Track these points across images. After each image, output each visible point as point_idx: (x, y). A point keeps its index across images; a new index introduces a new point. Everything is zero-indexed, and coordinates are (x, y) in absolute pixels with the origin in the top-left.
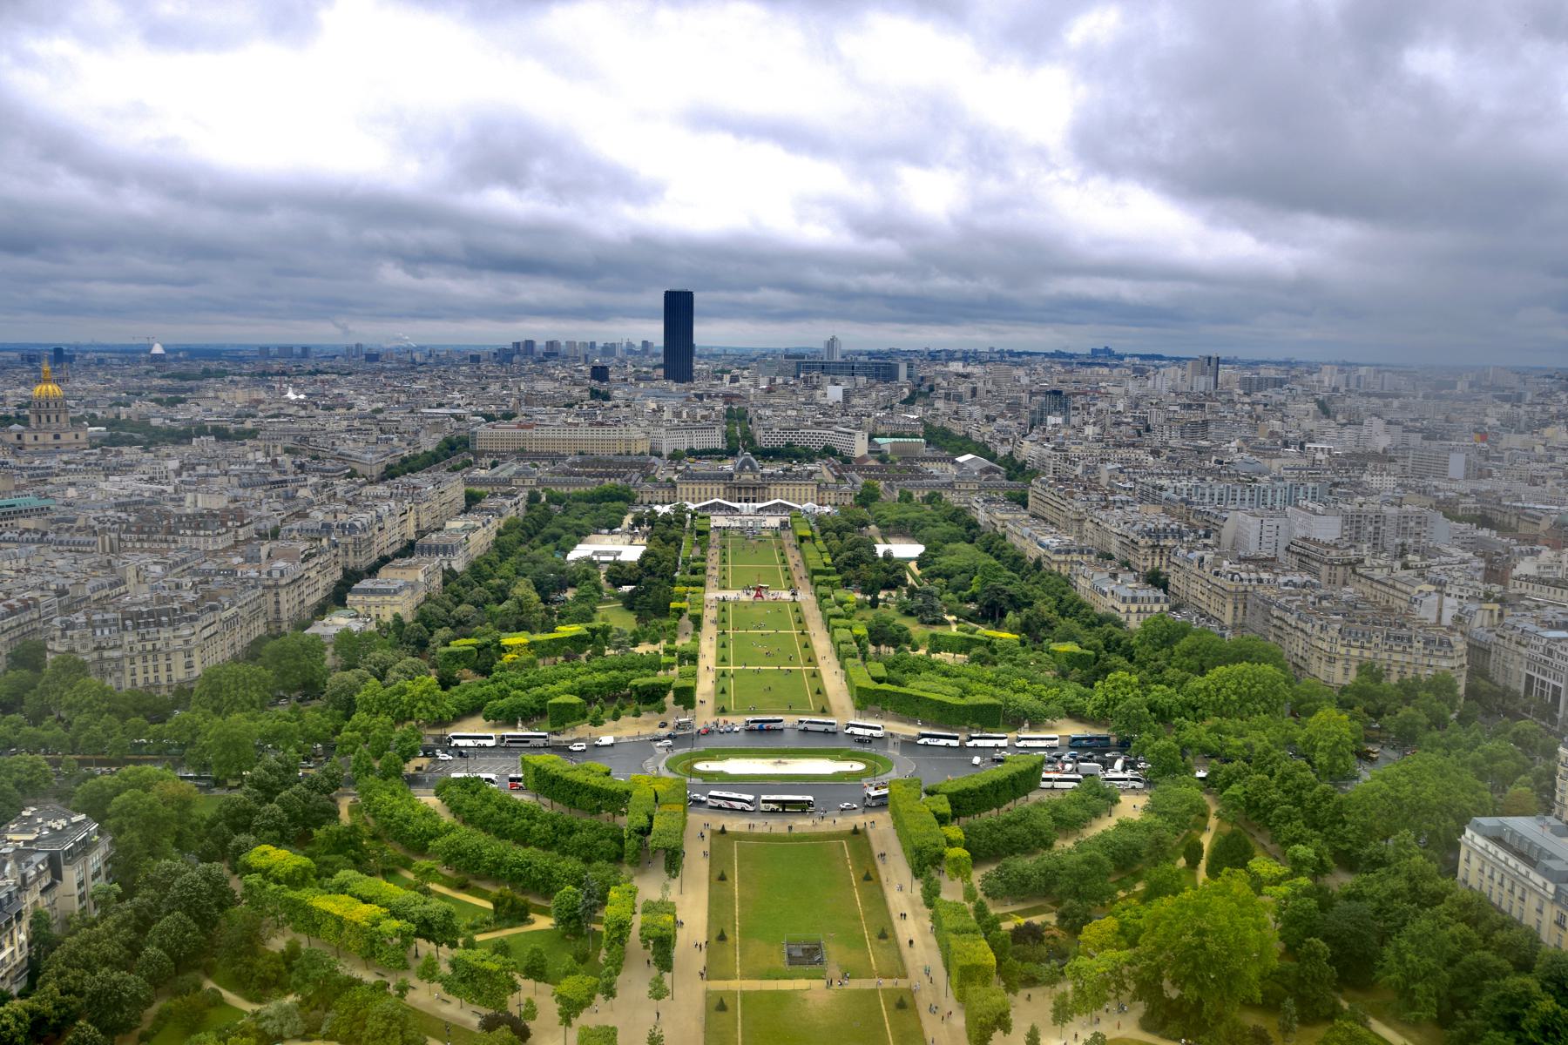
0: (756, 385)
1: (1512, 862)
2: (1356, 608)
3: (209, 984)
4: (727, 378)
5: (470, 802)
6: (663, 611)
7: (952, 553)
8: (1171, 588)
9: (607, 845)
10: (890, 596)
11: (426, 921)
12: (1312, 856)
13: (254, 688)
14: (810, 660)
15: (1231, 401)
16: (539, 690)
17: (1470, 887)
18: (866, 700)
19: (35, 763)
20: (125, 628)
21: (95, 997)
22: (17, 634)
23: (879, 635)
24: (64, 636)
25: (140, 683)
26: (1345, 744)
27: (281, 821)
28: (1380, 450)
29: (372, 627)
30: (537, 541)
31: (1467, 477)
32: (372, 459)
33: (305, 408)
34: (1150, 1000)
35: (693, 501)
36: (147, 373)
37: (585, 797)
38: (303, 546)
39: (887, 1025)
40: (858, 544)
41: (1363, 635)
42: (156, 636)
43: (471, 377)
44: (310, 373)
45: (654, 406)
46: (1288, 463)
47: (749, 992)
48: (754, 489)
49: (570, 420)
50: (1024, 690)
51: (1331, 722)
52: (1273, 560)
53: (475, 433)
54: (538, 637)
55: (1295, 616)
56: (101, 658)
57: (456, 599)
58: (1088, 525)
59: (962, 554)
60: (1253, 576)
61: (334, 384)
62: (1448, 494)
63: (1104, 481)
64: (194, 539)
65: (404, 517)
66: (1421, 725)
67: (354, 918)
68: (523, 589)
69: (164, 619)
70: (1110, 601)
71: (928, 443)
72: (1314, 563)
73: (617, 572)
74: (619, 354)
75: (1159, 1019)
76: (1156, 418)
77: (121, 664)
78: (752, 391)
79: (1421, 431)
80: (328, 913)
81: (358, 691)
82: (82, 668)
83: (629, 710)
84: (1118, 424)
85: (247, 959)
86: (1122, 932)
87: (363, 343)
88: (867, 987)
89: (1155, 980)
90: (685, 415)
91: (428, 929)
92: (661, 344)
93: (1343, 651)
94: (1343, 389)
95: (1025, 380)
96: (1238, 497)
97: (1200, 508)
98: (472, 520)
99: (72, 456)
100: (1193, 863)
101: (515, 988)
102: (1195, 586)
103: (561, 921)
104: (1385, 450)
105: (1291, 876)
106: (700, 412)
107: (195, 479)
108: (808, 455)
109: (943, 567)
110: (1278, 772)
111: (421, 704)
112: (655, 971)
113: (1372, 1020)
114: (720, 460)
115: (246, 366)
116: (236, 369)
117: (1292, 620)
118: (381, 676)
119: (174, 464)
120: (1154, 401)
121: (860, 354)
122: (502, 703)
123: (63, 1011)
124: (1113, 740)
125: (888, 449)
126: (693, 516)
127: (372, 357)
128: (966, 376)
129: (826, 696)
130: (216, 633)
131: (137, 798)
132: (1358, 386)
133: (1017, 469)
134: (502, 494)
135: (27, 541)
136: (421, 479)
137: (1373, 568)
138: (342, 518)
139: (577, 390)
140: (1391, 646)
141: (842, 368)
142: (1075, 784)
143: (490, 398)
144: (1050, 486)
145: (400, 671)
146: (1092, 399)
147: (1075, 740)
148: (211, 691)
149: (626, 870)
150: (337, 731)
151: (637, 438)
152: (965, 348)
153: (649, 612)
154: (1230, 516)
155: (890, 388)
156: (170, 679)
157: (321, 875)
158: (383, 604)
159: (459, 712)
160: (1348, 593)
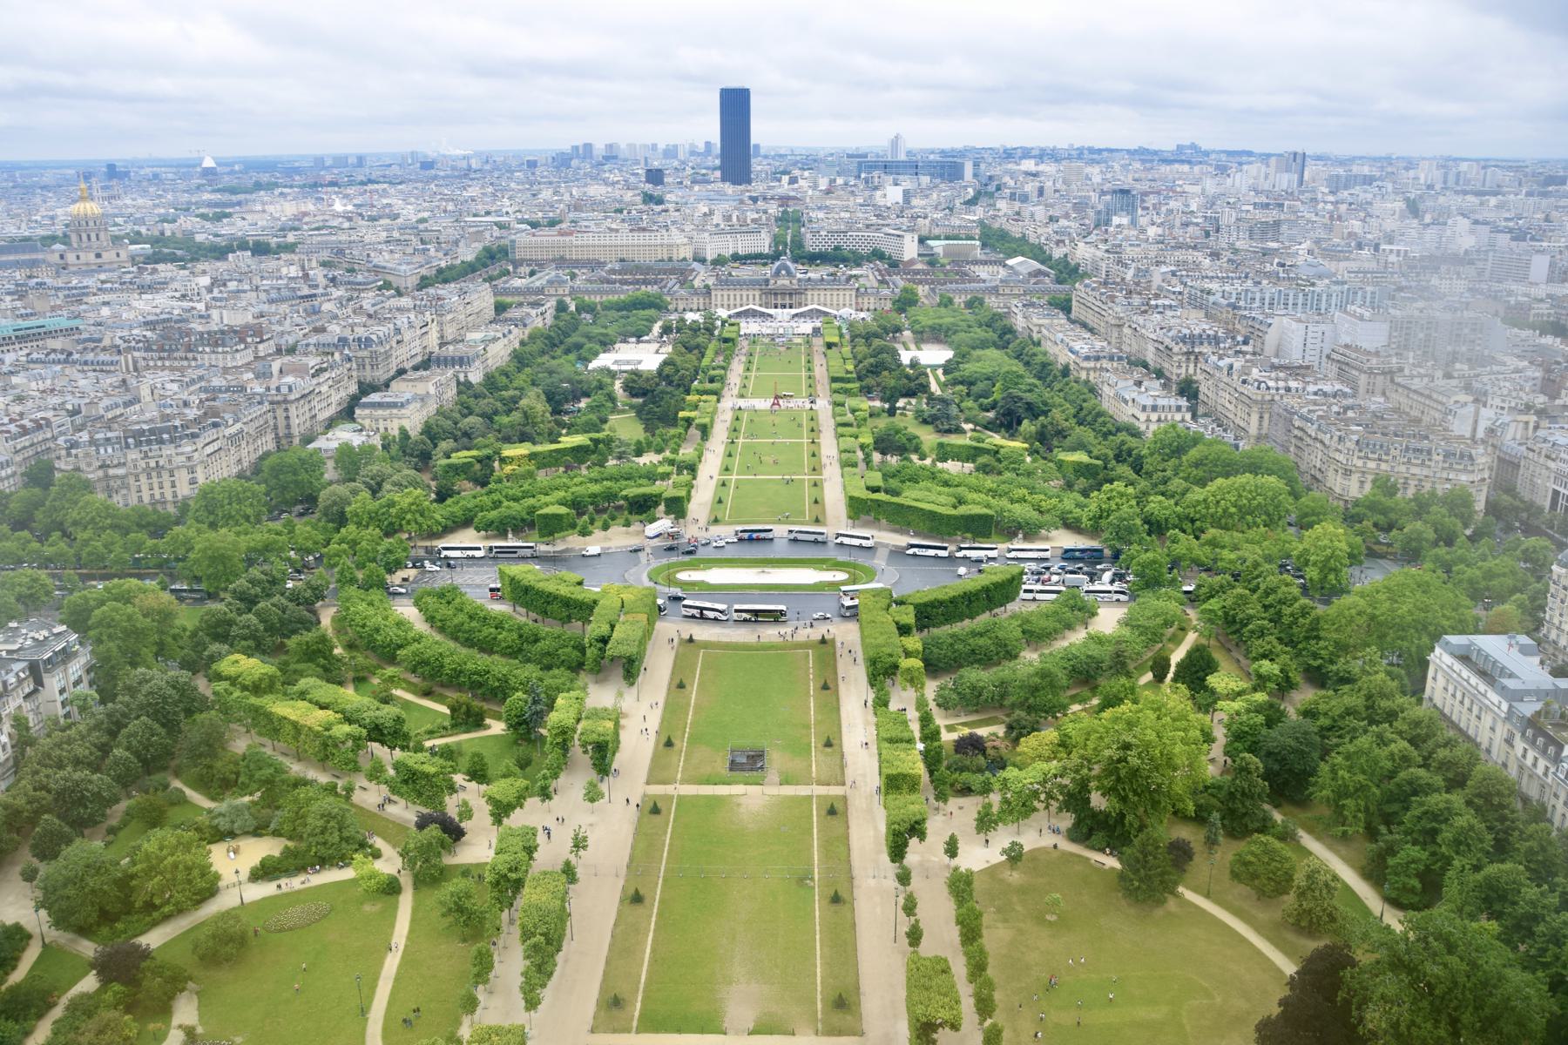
0: (815, 186)
1: (1474, 680)
2: (1382, 418)
3: (177, 784)
4: (786, 179)
5: (445, 611)
6: (672, 421)
7: (979, 359)
8: (1201, 396)
10: (910, 404)
11: (377, 725)
12: (1277, 672)
13: (247, 503)
14: (814, 470)
15: (1314, 200)
16: (531, 501)
17: (1435, 706)
19: (35, 576)
20: (128, 446)
21: (60, 795)
22: (31, 453)
23: (885, 444)
24: (69, 455)
25: (146, 499)
26: (1338, 559)
27: (257, 630)
28: (1462, 252)
29: (377, 441)
30: (559, 352)
31: (1550, 280)
32: (407, 271)
33: (350, 219)
34: (1075, 811)
35: (729, 308)
36: (198, 188)
37: (555, 607)
38: (313, 361)
39: (815, 830)
40: (881, 350)
41: (1381, 446)
42: (159, 453)
43: (523, 183)
44: (363, 183)
45: (706, 210)
46: (1354, 266)
48: (791, 294)
49: (614, 226)
50: (1023, 500)
51: (1331, 536)
52: (1308, 367)
53: (513, 241)
54: (539, 448)
55: (1315, 427)
56: (107, 476)
57: (466, 411)
58: (1126, 330)
60: (1281, 384)
61: (385, 194)
62: (1520, 298)
63: (1157, 280)
64: (213, 356)
65: (424, 330)
66: (1427, 540)
67: (308, 723)
68: (534, 401)
69: (165, 436)
70: (1130, 410)
71: (984, 246)
72: (1354, 372)
73: (634, 381)
74: (681, 156)
75: (1085, 830)
76: (1228, 217)
77: (126, 481)
79: (1511, 231)
81: (349, 504)
82: (88, 486)
83: (621, 521)
84: (1186, 225)
85: (207, 761)
86: (1063, 744)
88: (803, 793)
89: (1080, 792)
91: (377, 733)
92: (719, 145)
93: (1360, 463)
94: (1438, 187)
95: (1097, 179)
96: (1291, 302)
97: (1246, 313)
98: (496, 330)
100: (1160, 677)
101: (452, 789)
102: (1224, 394)
103: (510, 726)
104: (1466, 252)
105: (1255, 690)
106: (751, 215)
108: (856, 260)
109: (967, 373)
110: (1263, 586)
111: (409, 516)
112: (593, 775)
113: (1301, 832)
114: (765, 264)
115: (297, 178)
116: (288, 181)
117: (1312, 430)
118: (375, 490)
119: (205, 281)
120: (1232, 200)
121: (933, 153)
122: (493, 514)
123: (35, 805)
124: (1107, 552)
125: (940, 251)
126: (724, 322)
127: (428, 165)
128: (1035, 175)
129: (824, 505)
131: (116, 610)
132: (1457, 183)
133: (1068, 272)
135: (54, 362)
136: (449, 292)
137: (1412, 377)
138: (361, 332)
139: (630, 193)
140: (1409, 459)
142: (1054, 596)
143: (538, 205)
144: (1093, 289)
145: (395, 484)
146: (1165, 198)
147: (1067, 551)
149: (583, 678)
150: (328, 543)
151: (678, 242)
152: (1043, 145)
153: (656, 422)
154: (1275, 321)
155: (954, 188)
156: (175, 495)
157: (281, 684)
158: (391, 417)
159: (449, 523)
160: (1376, 402)
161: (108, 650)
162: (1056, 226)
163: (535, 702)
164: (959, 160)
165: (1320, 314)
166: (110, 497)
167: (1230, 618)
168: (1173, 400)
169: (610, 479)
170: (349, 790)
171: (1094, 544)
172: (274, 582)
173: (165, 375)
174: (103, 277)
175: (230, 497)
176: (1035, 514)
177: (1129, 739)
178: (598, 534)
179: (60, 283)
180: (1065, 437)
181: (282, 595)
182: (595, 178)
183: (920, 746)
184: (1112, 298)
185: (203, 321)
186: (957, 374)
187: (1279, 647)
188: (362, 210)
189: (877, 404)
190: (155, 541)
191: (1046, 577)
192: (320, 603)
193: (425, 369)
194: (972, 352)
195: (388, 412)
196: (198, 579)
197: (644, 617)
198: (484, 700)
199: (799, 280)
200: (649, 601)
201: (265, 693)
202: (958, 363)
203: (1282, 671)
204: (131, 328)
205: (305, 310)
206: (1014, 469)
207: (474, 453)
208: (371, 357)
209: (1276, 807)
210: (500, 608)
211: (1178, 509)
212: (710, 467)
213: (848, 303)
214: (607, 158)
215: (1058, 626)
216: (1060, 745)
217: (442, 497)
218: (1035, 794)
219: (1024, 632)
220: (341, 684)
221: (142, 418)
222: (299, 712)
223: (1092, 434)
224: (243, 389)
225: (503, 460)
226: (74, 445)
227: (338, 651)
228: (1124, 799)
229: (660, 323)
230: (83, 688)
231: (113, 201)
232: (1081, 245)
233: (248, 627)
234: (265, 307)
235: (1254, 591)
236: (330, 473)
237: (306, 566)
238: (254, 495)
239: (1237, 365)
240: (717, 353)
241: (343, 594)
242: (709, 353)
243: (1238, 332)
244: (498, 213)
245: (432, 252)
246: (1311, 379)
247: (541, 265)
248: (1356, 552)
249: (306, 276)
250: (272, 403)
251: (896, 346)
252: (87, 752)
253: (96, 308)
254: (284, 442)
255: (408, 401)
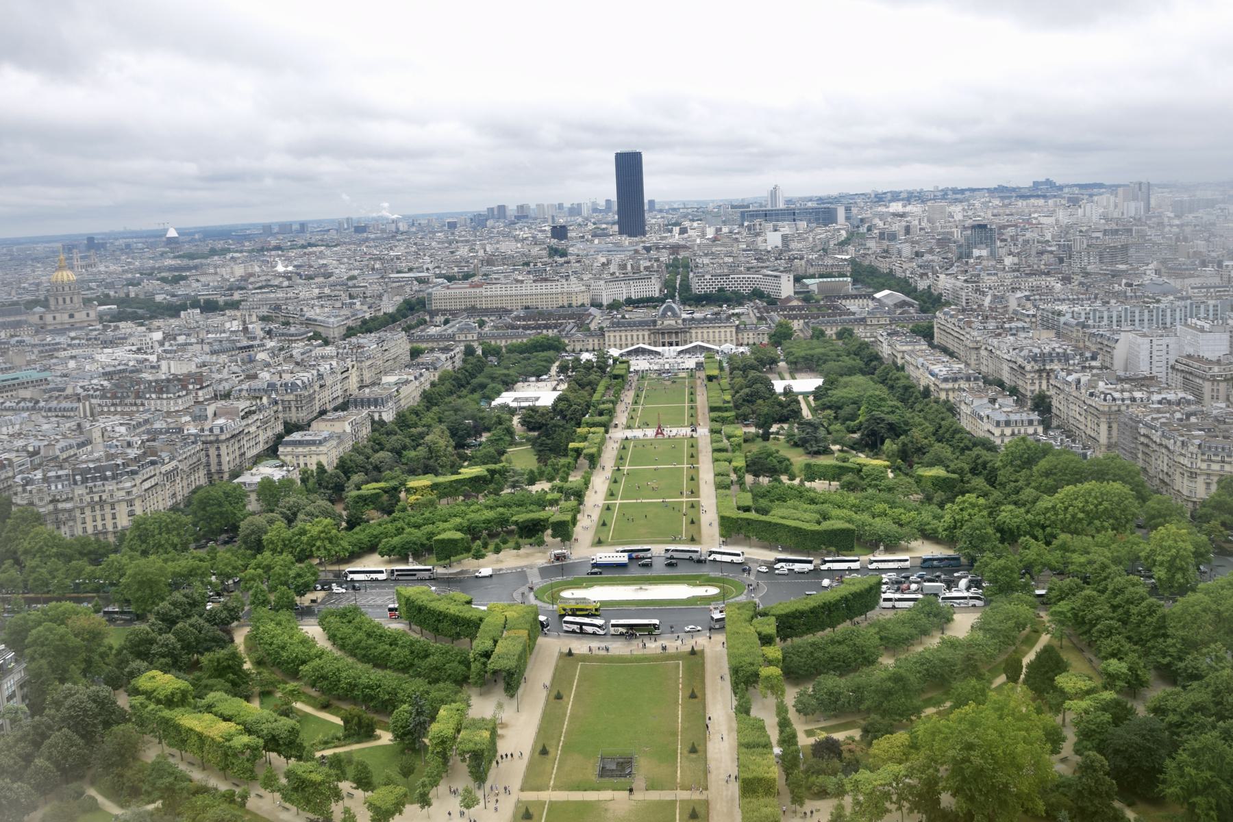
0: (703, 235)
2: (1225, 423)
3: (92, 792)
4: (676, 229)
5: (346, 629)
7: (846, 385)
8: (1054, 410)
9: (455, 667)
10: (782, 428)
11: (274, 736)
16: (429, 528)
18: (731, 529)
20: (75, 483)
24: (24, 491)
25: (90, 530)
26: (1183, 558)
27: (174, 649)
29: (296, 476)
30: (465, 392)
32: (332, 319)
33: (289, 279)
36: (162, 255)
37: (444, 625)
38: (243, 405)
40: (755, 381)
41: (1223, 449)
43: (443, 243)
44: (303, 247)
45: (604, 260)
47: (556, 802)
48: (677, 333)
49: (520, 278)
52: (1152, 378)
53: (430, 294)
54: (441, 479)
55: (1159, 433)
56: (56, 509)
57: (377, 447)
58: (983, 353)
59: (858, 386)
60: (1126, 395)
61: (321, 255)
63: (1013, 304)
64: (159, 402)
65: (345, 375)
68: (438, 437)
69: (108, 473)
71: (855, 282)
72: (1197, 380)
73: (531, 416)
74: (585, 213)
76: (1080, 244)
78: (698, 241)
80: (192, 730)
81: (266, 533)
82: (39, 519)
83: (511, 544)
84: (1041, 253)
87: (351, 216)
88: (668, 798)
90: (629, 267)
91: (273, 743)
93: (1204, 466)
95: (958, 217)
96: (1137, 319)
97: (1094, 331)
99: (79, 333)
101: (338, 796)
102: (1074, 407)
103: (396, 737)
105: (1105, 688)
107: (175, 348)
108: (737, 299)
109: (834, 399)
110: (1110, 587)
111: (318, 543)
114: (655, 307)
115: (247, 244)
117: (1156, 436)
118: (290, 521)
119: (158, 336)
120: (1084, 229)
121: (811, 200)
122: (396, 540)
125: (814, 288)
127: (360, 229)
128: (902, 215)
130: (157, 484)
131: (50, 630)
133: (931, 302)
134: (440, 349)
135: (23, 409)
136: (369, 341)
138: (287, 377)
139: (537, 248)
141: (783, 214)
142: (911, 603)
144: (952, 316)
145: (307, 514)
147: (925, 560)
148: (140, 536)
150: (246, 567)
151: (572, 290)
152: (910, 189)
156: (115, 526)
159: (356, 549)
161: (40, 668)
162: (920, 260)
163: (419, 714)
164: (832, 206)
165: (1165, 328)
166: (58, 528)
167: (1080, 619)
168: (1024, 414)
169: (505, 505)
170: (244, 797)
171: (949, 552)
172: (194, 604)
173: (117, 419)
174: (73, 334)
175: (160, 528)
176: (895, 527)
177: (971, 738)
178: (491, 557)
179: (36, 340)
180: (924, 454)
181: (201, 616)
182: (507, 235)
183: (777, 750)
184: (969, 324)
185: (154, 371)
186: (825, 400)
187: (1127, 646)
188: (301, 271)
189: (753, 430)
190: (93, 568)
191: (905, 586)
192: (235, 623)
193: (343, 411)
194: (840, 379)
195: (307, 449)
196: (128, 602)
197: (524, 633)
198: (377, 712)
199: (684, 320)
200: (530, 617)
201: (177, 706)
202: (827, 389)
203: (1130, 669)
204: (92, 378)
205: (242, 360)
206: (876, 486)
207: (382, 484)
208: (297, 401)
209: (1129, 805)
210: (396, 626)
211: (1029, 516)
212: (596, 495)
213: (729, 339)
214: (518, 218)
215: (914, 631)
216: (911, 747)
217: (351, 525)
218: (887, 796)
219: (881, 639)
220: (248, 699)
221: (91, 457)
222: (204, 724)
223: (950, 450)
224: (180, 430)
225: (408, 491)
226: (28, 482)
227: (247, 666)
228: (971, 799)
229: (557, 364)
230: (16, 703)
231: (89, 269)
232: (942, 277)
233: (167, 645)
234: (207, 358)
235: (1103, 592)
236: (253, 504)
237: (227, 589)
238: (182, 525)
239: (1084, 380)
240: (607, 388)
241: (255, 615)
242: (600, 389)
243: (1088, 348)
244: (420, 269)
245: (358, 305)
246: (1156, 389)
247: (454, 314)
248: (1202, 550)
249: (245, 330)
250: (204, 443)
251: (770, 376)
252: (12, 762)
253: (64, 361)
254: (216, 477)
255: (325, 440)
